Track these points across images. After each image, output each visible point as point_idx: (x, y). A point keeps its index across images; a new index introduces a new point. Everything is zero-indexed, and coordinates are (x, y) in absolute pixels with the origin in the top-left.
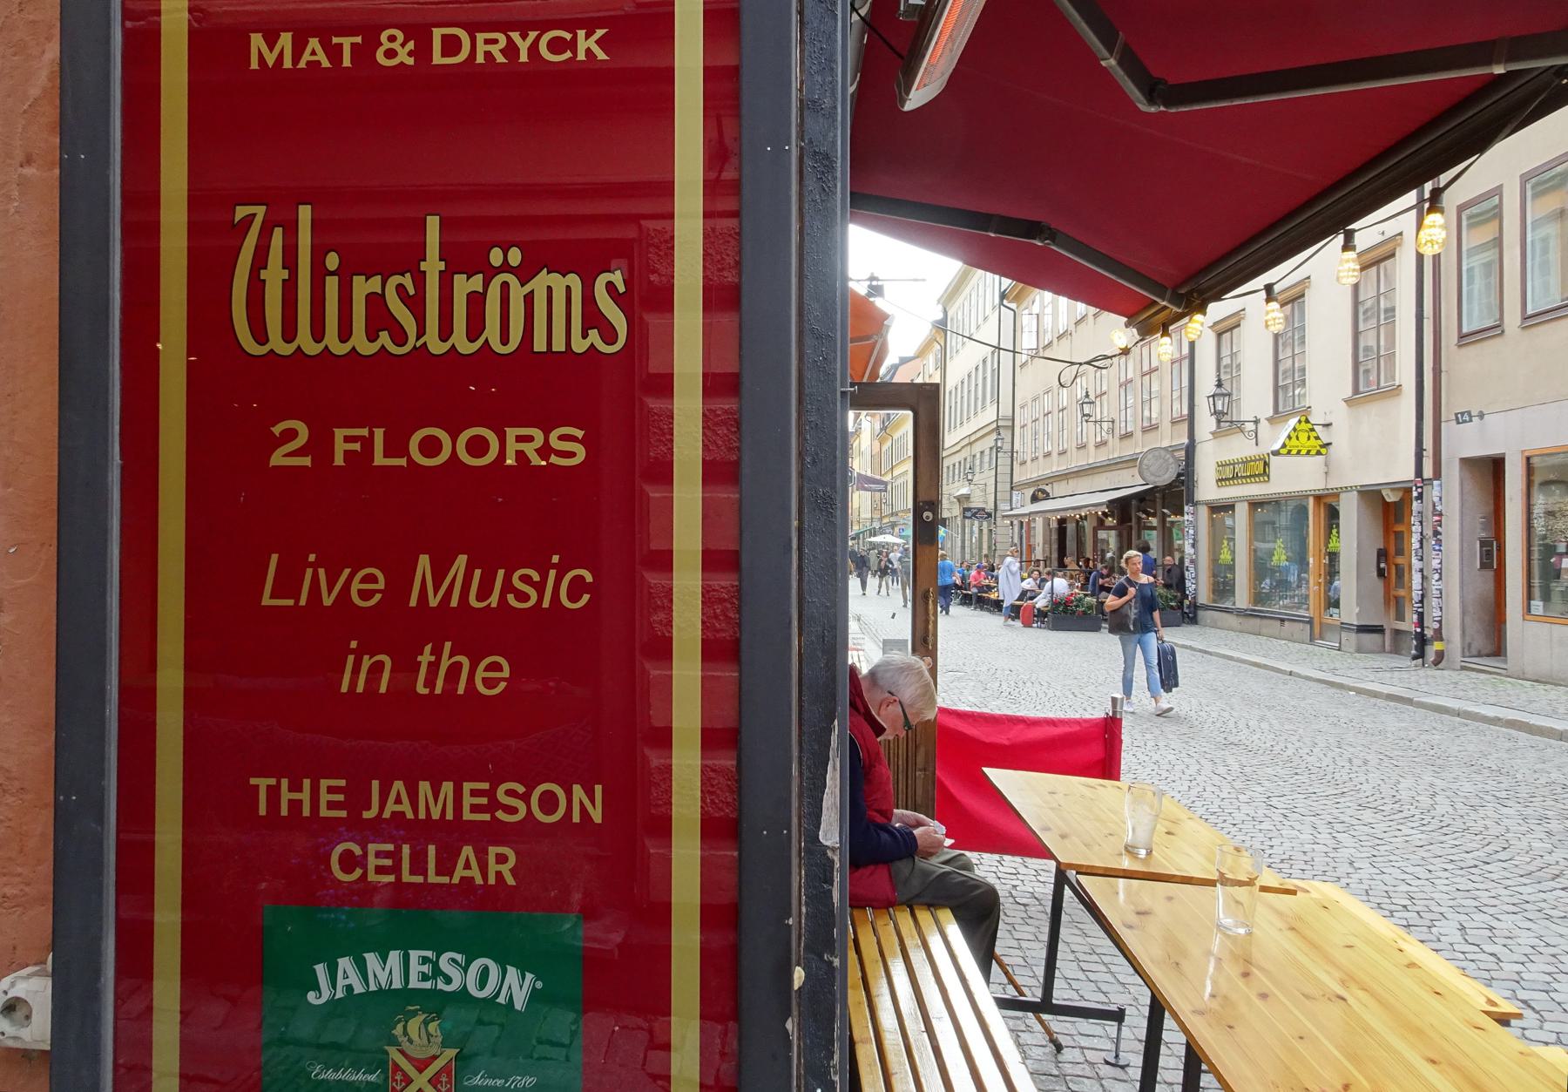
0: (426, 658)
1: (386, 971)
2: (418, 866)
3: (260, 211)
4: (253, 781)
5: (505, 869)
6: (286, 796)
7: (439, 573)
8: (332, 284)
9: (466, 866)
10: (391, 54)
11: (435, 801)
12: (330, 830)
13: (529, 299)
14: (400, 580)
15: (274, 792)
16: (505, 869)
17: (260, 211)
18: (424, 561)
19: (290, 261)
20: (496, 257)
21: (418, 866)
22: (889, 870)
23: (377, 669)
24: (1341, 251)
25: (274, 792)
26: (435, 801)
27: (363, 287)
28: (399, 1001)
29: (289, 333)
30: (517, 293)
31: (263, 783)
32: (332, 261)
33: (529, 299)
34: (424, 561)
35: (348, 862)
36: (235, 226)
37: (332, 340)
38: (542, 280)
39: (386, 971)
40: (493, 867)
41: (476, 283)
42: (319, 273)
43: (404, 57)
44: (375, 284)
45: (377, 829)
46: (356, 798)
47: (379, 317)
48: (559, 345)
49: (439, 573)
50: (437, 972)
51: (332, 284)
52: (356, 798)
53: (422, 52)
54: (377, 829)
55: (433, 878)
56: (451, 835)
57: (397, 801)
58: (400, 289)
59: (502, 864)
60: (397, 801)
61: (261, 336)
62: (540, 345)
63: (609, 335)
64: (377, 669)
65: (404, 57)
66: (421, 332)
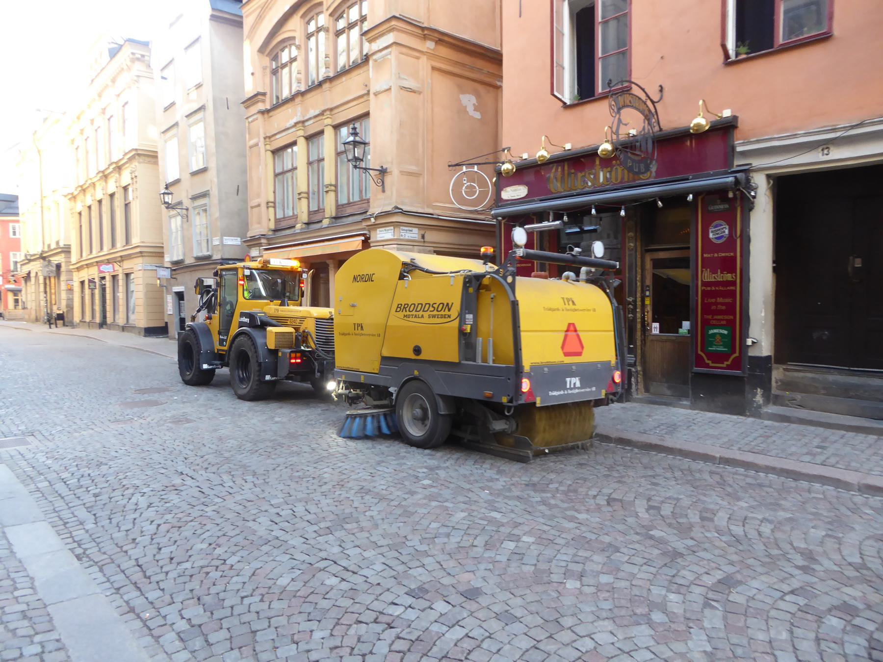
1: (715, 331)
12: (710, 320)
28: (715, 334)
39: (715, 331)
47: (715, 278)
60: (716, 317)
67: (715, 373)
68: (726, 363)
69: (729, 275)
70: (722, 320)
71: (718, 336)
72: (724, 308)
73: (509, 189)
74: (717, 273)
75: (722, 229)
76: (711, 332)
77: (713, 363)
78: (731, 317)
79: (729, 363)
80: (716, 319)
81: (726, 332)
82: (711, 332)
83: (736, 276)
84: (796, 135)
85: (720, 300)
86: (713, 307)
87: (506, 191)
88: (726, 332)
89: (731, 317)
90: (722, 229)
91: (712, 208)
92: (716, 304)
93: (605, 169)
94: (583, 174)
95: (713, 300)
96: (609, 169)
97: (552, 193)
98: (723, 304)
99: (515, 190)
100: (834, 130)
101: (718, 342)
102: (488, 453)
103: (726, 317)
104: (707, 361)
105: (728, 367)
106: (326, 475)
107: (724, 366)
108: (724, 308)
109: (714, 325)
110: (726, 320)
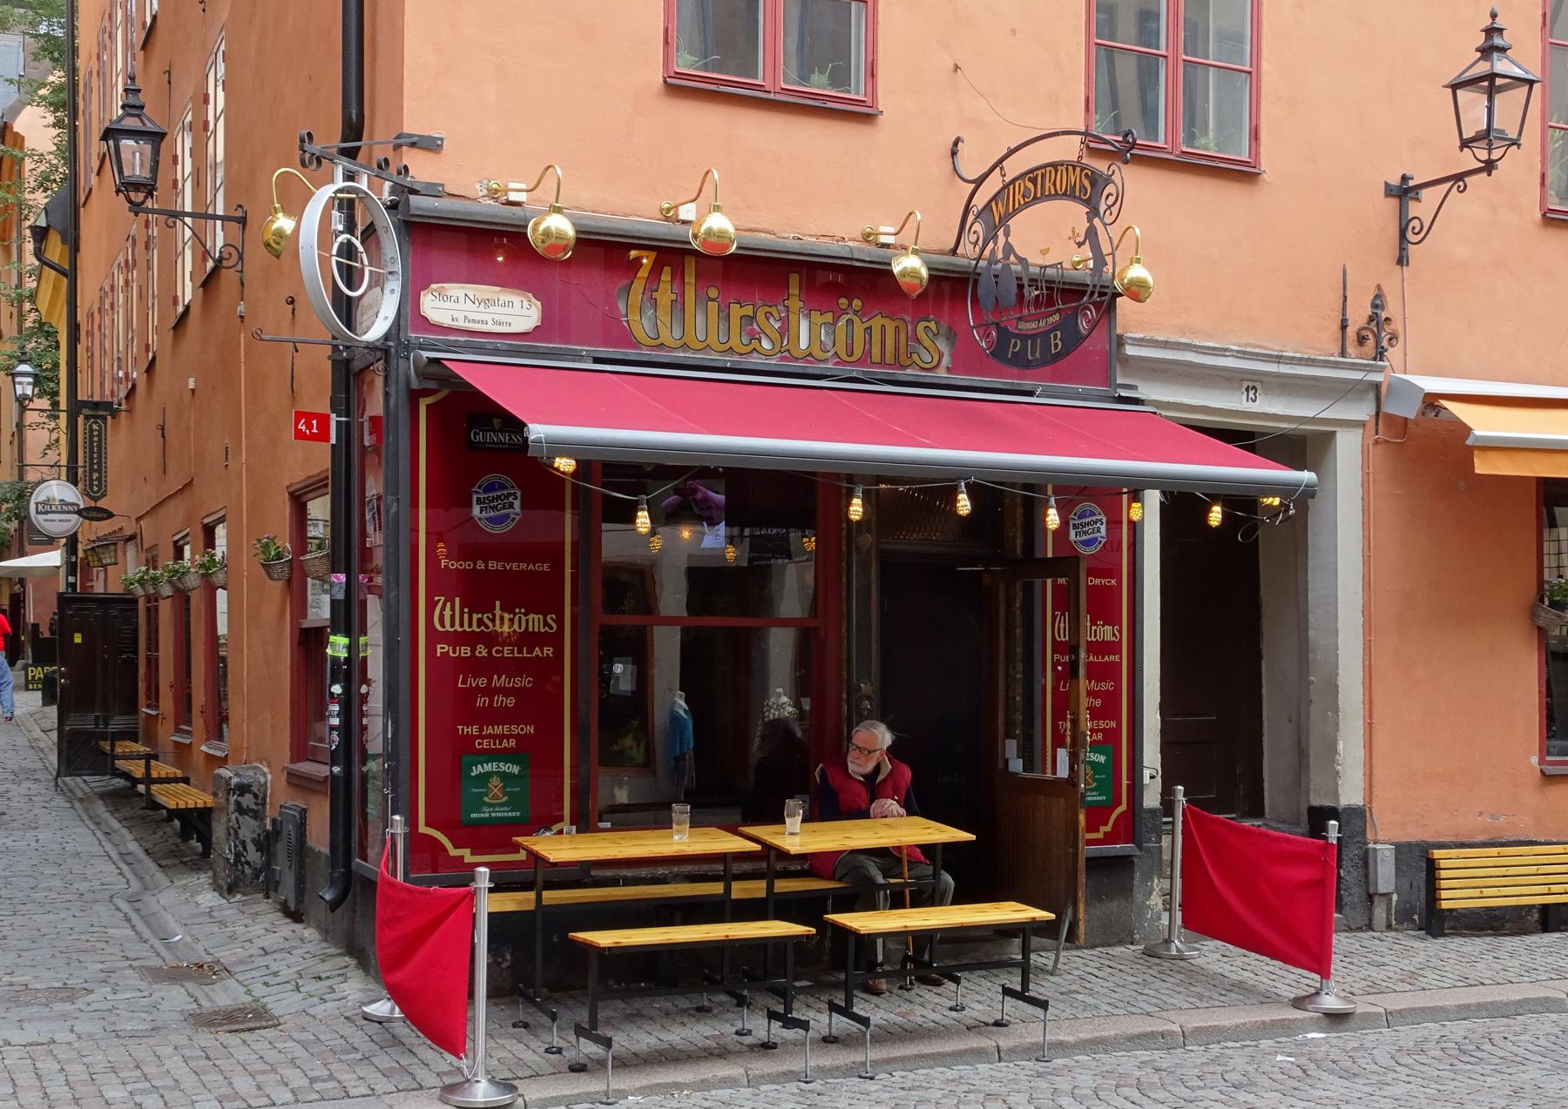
0: (496, 698)
1: (488, 767)
2: (495, 744)
3: (443, 598)
4: (439, 655)
5: (550, 653)
6: (466, 730)
7: (499, 679)
8: (466, 616)
9: (505, 744)
10: (480, 653)
11: (498, 730)
12: (475, 737)
13: (527, 620)
14: (490, 681)
15: (463, 729)
16: (550, 653)
17: (443, 598)
18: (495, 676)
19: (453, 609)
20: (517, 610)
21: (495, 744)
22: (1497, 160)
23: (485, 701)
24: (1458, 150)
25: (463, 729)
26: (498, 730)
27: (475, 617)
28: (489, 775)
29: (453, 625)
30: (524, 619)
31: (460, 727)
32: (466, 610)
33: (527, 620)
34: (495, 676)
35: (479, 744)
36: (496, 884)
37: (466, 627)
38: (530, 617)
39: (488, 767)
40: (545, 652)
41: (512, 616)
42: (462, 613)
43: (483, 567)
44: (480, 616)
45: (487, 736)
46: (481, 730)
47: (480, 622)
48: (536, 630)
49: (499, 679)
50: (499, 767)
51: (466, 616)
52: (481, 730)
53: (489, 652)
54: (487, 736)
55: (516, 655)
56: (502, 737)
57: (490, 730)
58: (488, 617)
59: (513, 743)
60: (489, 730)
61: (443, 625)
62: (530, 630)
63: (551, 628)
64: (485, 701)
65: (484, 654)
66: (494, 626)
67: (1113, 853)
68: (1103, 829)
69: (1108, 628)
70: (508, 737)
71: (495, 781)
72: (510, 702)
73: (455, 290)
74: (492, 609)
75: (507, 496)
76: (478, 770)
77: (473, 854)
78: (1113, 724)
79: (1108, 828)
80: (490, 736)
81: (515, 769)
82: (478, 770)
83: (1120, 631)
84: (1226, 350)
85: (499, 681)
86: (481, 701)
87: (441, 295)
88: (515, 769)
89: (1113, 724)
90: (507, 496)
91: (480, 438)
92: (490, 692)
93: (815, 315)
94: (748, 310)
95: (482, 682)
96: (829, 317)
97: (636, 344)
98: (506, 692)
99: (487, 302)
100: (1278, 359)
101: (495, 797)
102: (930, 1037)
103: (515, 730)
104: (453, 852)
105: (1109, 839)
106: (937, 1082)
107: (1100, 835)
108: (510, 702)
109: (483, 751)
110: (517, 737)
